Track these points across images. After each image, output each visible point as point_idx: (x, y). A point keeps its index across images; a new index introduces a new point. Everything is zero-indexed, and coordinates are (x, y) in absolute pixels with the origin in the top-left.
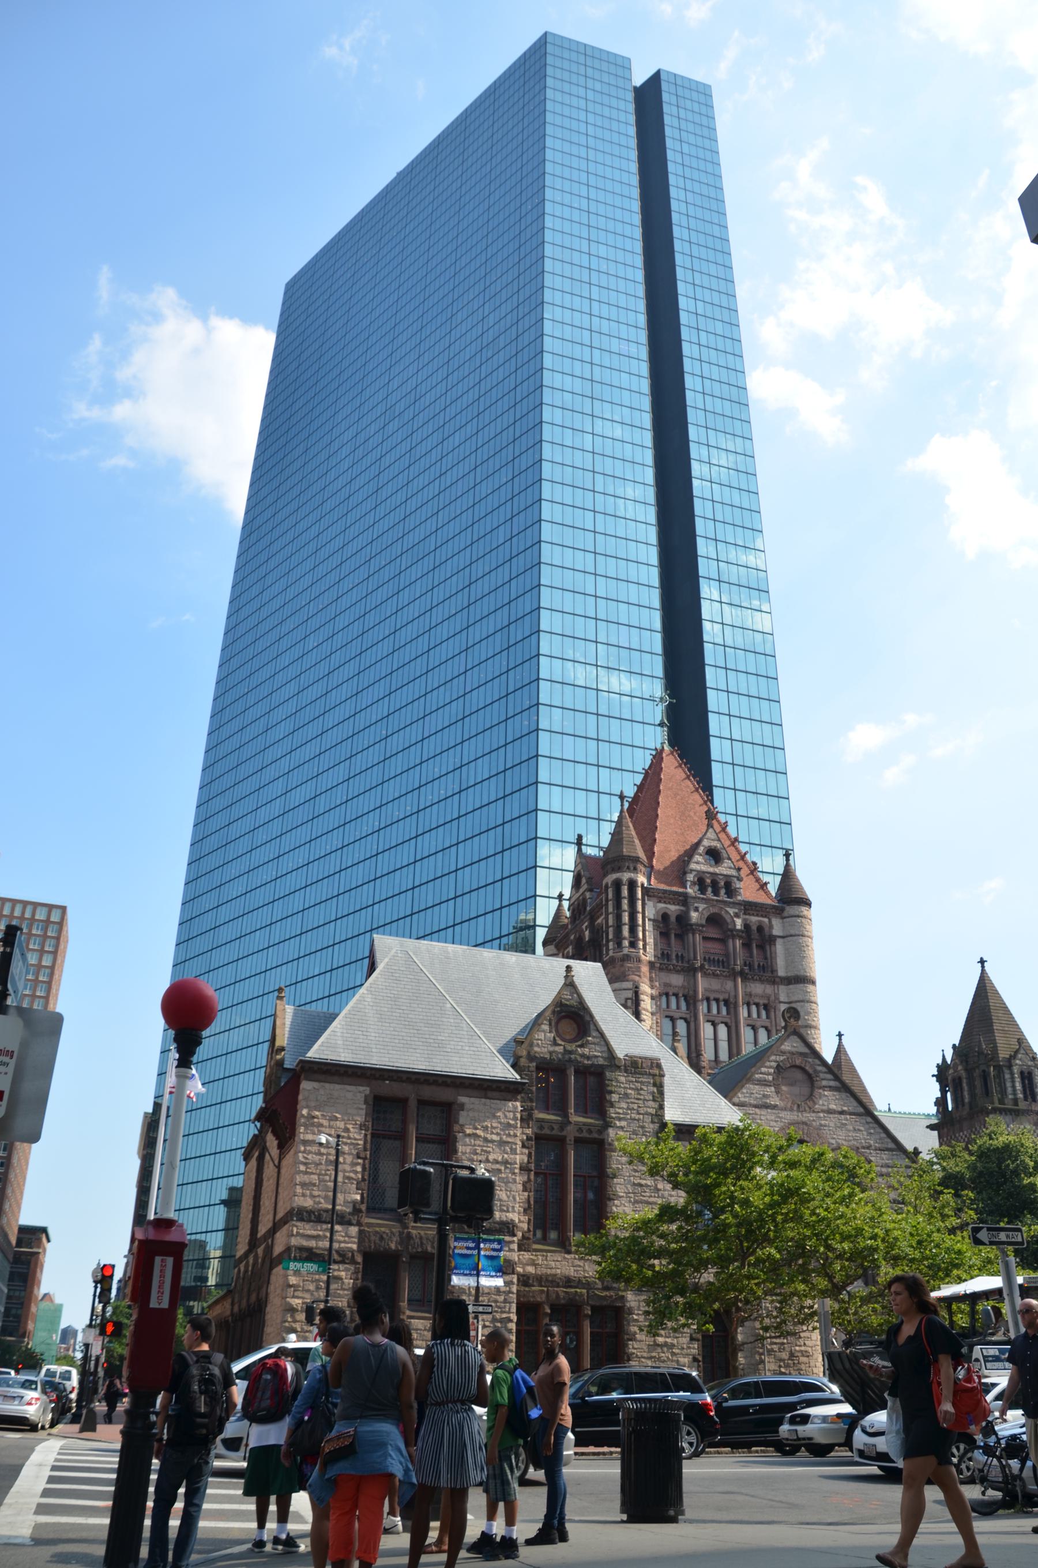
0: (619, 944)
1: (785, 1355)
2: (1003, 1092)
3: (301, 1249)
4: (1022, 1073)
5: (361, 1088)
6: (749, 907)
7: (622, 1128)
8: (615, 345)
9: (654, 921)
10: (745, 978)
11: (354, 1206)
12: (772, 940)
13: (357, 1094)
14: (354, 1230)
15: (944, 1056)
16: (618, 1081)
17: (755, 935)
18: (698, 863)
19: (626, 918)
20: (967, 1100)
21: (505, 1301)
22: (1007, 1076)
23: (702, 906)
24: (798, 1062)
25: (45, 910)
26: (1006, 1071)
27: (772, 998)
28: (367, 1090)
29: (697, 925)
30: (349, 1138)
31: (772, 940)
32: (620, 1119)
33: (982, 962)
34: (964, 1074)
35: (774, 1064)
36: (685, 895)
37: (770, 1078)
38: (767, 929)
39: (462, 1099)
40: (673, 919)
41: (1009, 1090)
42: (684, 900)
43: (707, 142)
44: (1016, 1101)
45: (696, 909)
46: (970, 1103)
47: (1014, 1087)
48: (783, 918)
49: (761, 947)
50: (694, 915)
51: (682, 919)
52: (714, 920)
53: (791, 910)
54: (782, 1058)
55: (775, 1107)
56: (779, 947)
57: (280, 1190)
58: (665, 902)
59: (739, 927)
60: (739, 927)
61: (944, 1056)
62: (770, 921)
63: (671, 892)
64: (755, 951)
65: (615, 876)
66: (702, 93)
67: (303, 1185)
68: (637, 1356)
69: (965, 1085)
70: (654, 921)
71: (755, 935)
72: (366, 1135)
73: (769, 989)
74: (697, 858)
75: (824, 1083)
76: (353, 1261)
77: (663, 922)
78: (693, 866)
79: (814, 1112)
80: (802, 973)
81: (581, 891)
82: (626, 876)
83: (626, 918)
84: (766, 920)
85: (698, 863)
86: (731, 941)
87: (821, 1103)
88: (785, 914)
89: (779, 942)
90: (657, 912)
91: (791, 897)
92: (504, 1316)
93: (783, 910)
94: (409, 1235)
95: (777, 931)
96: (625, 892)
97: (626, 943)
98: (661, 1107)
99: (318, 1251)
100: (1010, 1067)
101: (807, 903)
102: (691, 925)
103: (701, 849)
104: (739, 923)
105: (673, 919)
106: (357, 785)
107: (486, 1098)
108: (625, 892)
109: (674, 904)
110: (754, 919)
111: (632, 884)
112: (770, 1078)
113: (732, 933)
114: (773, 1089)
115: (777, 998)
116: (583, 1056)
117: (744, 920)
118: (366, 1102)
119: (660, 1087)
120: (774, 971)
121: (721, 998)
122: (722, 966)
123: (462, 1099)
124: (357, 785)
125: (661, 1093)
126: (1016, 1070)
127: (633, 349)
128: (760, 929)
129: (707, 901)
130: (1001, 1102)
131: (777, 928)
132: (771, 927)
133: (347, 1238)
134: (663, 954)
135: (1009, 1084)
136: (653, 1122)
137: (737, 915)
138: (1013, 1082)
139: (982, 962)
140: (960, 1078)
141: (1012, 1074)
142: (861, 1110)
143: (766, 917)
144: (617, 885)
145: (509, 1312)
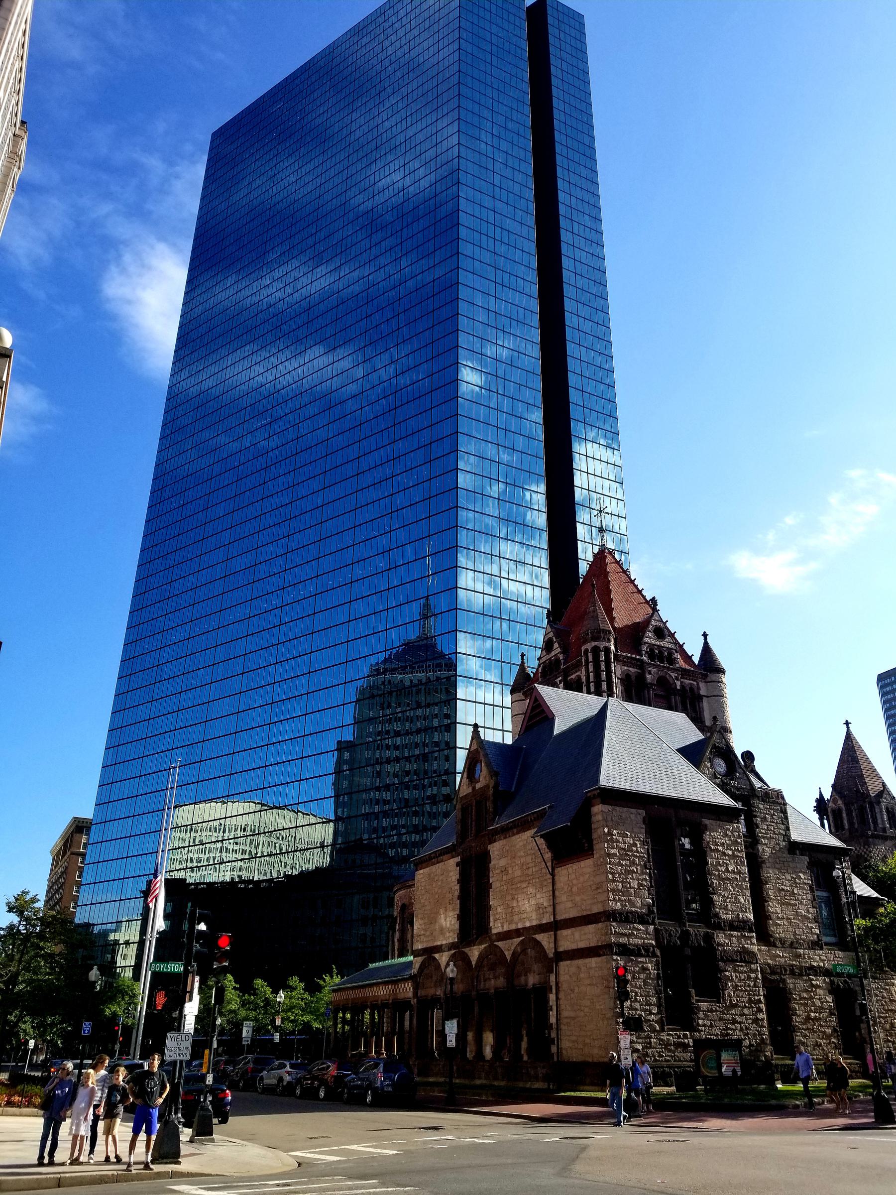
1: (888, 1026)
2: (875, 822)
3: (620, 945)
4: (887, 809)
5: (640, 811)
6: (684, 673)
7: (766, 844)
8: (511, 225)
11: (649, 908)
12: (701, 698)
13: (636, 815)
14: (651, 928)
16: (758, 808)
18: (649, 637)
19: (604, 676)
21: (755, 986)
22: (877, 810)
23: (653, 670)
28: (643, 812)
29: (651, 684)
30: (637, 852)
31: (701, 698)
32: (764, 838)
33: (847, 723)
34: (843, 806)
36: (642, 661)
39: (706, 822)
41: (879, 821)
42: (641, 665)
43: (580, 63)
44: (884, 830)
45: (650, 673)
46: (849, 829)
48: (706, 682)
53: (712, 676)
56: (705, 703)
57: (557, 893)
62: (698, 684)
63: (632, 658)
65: (594, 644)
66: (576, 20)
67: (613, 891)
68: (799, 1028)
69: (844, 815)
72: (648, 849)
74: (648, 634)
76: (654, 955)
78: (646, 640)
81: (553, 653)
82: (602, 644)
83: (604, 676)
85: (649, 637)
88: (709, 679)
89: (705, 700)
90: (623, 672)
91: (709, 665)
92: (757, 998)
93: (706, 676)
94: (688, 932)
95: (702, 692)
96: (602, 657)
98: (788, 829)
99: (631, 947)
100: (879, 803)
101: (722, 671)
102: (647, 684)
105: (633, 678)
107: (720, 820)
108: (602, 657)
110: (687, 682)
111: (607, 650)
116: (734, 787)
117: (681, 682)
118: (644, 822)
119: (784, 812)
123: (706, 822)
125: (786, 818)
126: (883, 805)
127: (525, 231)
128: (691, 689)
129: (656, 666)
130: (875, 830)
132: (699, 688)
133: (642, 935)
136: (784, 841)
137: (677, 679)
138: (882, 815)
139: (847, 723)
140: (840, 810)
144: (596, 650)
145: (759, 995)
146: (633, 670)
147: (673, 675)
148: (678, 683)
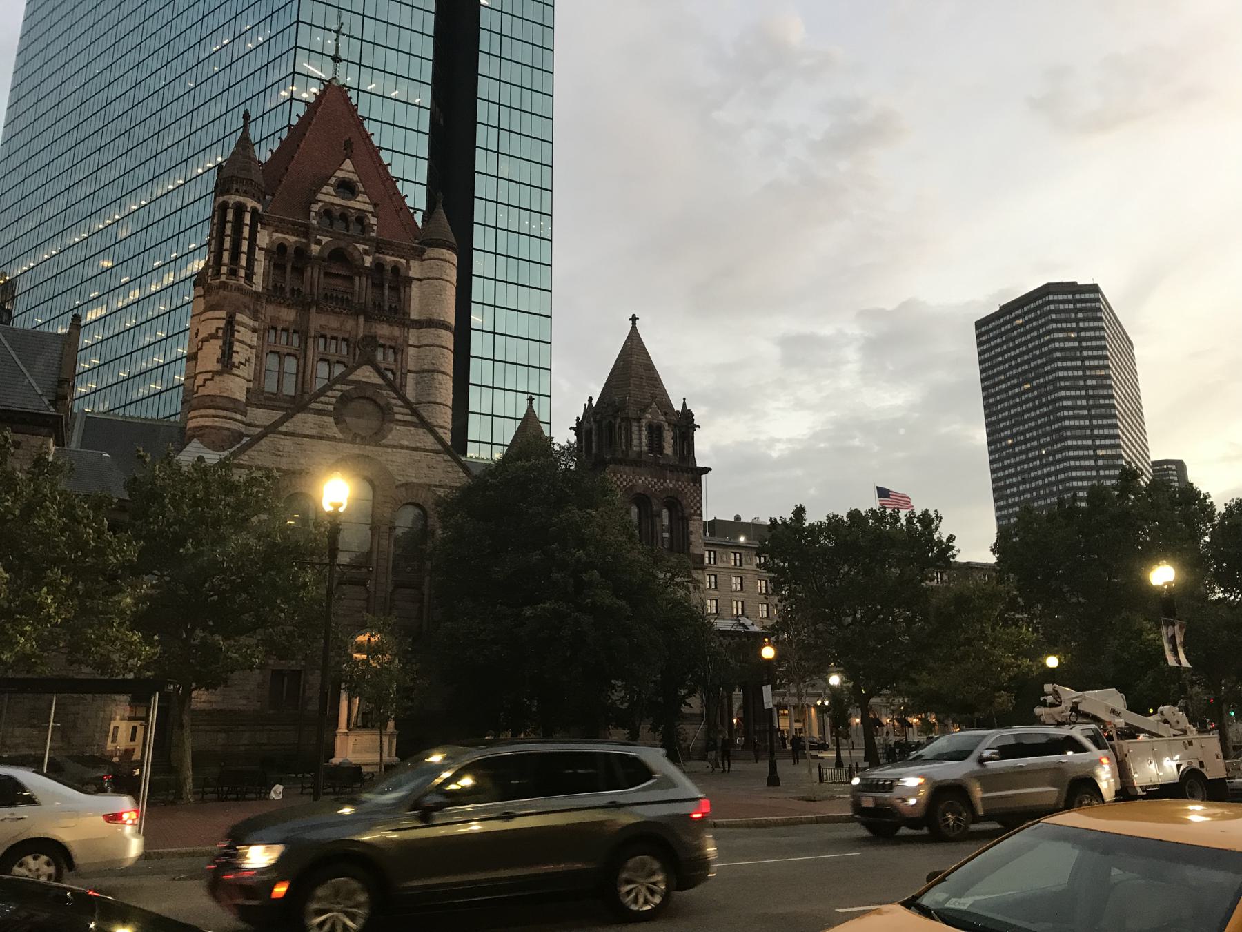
0: (233, 273)
9: (266, 250)
10: (368, 319)
12: (409, 281)
15: (684, 404)
17: (388, 275)
20: (594, 451)
22: (635, 429)
23: (325, 240)
24: (368, 394)
25: (143, 714)
26: (635, 424)
27: (400, 341)
31: (409, 281)
35: (339, 394)
37: (331, 408)
38: (402, 272)
40: (291, 251)
41: (635, 442)
45: (318, 242)
47: (640, 439)
49: (395, 289)
50: (315, 249)
51: (301, 252)
52: (338, 255)
54: (348, 388)
55: (333, 439)
56: (415, 288)
58: (282, 232)
59: (367, 264)
60: (367, 264)
61: (684, 404)
62: (408, 263)
64: (386, 292)
70: (266, 250)
71: (388, 275)
73: (396, 331)
75: (398, 417)
77: (277, 253)
78: (320, 197)
79: (380, 446)
80: (435, 317)
84: (403, 261)
86: (357, 278)
87: (391, 438)
88: (426, 256)
89: (415, 285)
90: (272, 242)
93: (423, 251)
96: (230, 217)
97: (224, 270)
103: (333, 180)
104: (368, 261)
105: (291, 251)
106: (256, 84)
109: (293, 234)
112: (331, 408)
113: (360, 270)
114: (332, 419)
115: (406, 340)
120: (406, 314)
121: (340, 337)
122: (343, 304)
124: (256, 84)
128: (396, 269)
131: (415, 270)
132: (409, 268)
134: (275, 286)
135: (635, 436)
137: (366, 252)
141: (640, 427)
142: (440, 447)
143: (402, 257)
146: (292, 239)
147: (361, 247)
148: (368, 261)
